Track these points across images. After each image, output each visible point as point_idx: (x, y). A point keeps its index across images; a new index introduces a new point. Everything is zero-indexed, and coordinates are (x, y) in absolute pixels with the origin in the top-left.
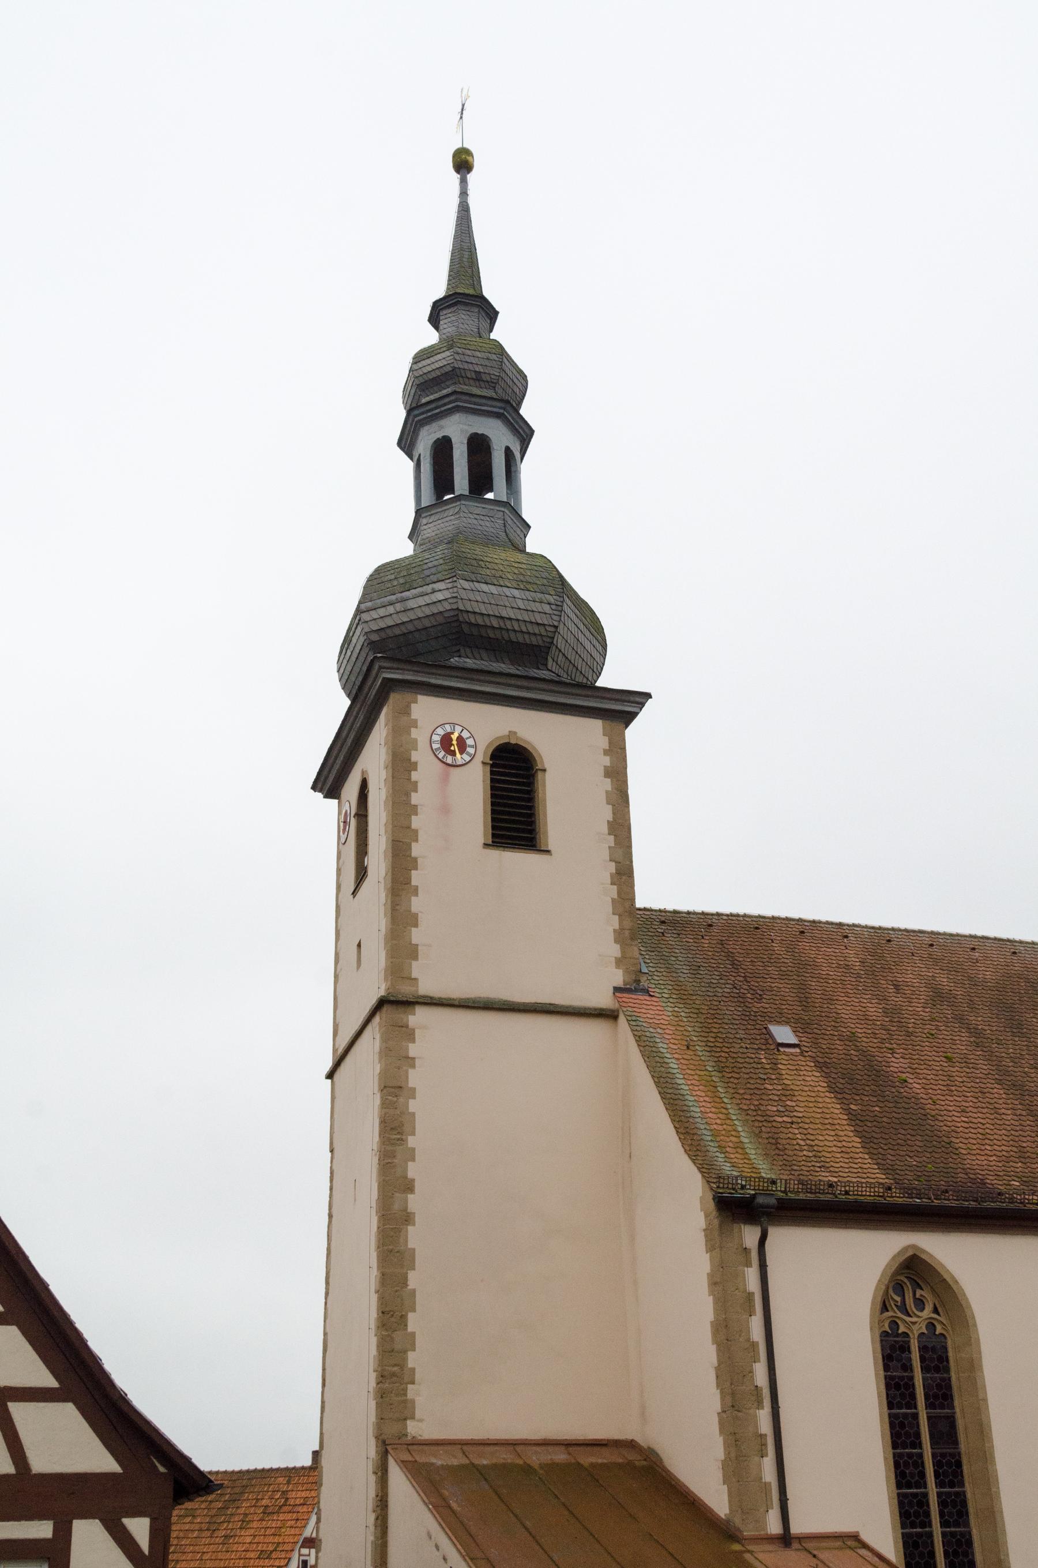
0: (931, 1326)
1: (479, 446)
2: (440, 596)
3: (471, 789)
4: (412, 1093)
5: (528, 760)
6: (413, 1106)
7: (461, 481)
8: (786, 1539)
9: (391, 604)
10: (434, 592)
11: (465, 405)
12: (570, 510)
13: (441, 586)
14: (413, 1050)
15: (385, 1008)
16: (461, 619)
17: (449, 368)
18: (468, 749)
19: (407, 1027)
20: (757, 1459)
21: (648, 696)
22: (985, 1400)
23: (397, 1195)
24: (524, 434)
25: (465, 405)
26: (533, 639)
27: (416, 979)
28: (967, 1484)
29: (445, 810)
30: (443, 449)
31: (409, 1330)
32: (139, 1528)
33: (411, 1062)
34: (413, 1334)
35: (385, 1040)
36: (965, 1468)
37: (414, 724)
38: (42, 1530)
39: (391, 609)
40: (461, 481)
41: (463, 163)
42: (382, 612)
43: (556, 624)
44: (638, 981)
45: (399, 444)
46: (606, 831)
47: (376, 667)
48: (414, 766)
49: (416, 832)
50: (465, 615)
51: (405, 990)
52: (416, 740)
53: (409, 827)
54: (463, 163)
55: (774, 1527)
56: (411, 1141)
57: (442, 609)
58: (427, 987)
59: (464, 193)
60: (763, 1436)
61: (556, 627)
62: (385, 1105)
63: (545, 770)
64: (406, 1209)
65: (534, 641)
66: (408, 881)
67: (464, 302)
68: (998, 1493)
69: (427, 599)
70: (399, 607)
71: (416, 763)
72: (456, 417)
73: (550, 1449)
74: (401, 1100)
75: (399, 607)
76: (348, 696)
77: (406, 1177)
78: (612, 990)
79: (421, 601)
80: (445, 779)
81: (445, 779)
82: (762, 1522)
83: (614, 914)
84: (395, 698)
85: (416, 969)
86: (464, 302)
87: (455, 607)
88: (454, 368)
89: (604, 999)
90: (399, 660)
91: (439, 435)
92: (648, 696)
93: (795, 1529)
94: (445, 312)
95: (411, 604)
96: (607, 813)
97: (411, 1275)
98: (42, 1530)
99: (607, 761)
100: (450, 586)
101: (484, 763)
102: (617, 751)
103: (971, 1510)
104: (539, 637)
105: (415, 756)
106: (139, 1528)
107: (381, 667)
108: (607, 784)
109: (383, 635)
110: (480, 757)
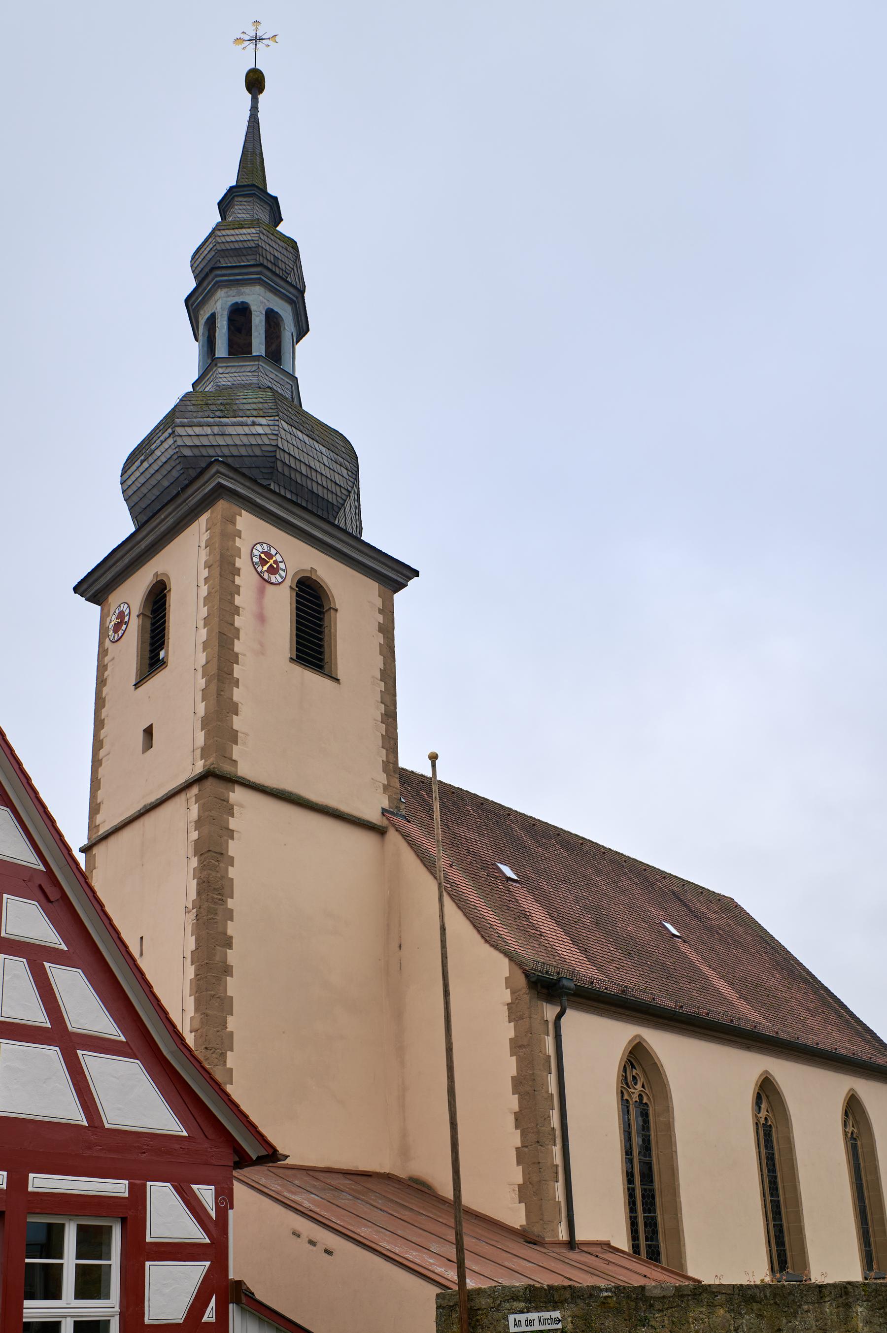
0: (640, 1096)
1: (272, 319)
2: (260, 430)
3: (281, 605)
4: (231, 861)
5: (318, 598)
6: (232, 872)
7: (258, 346)
8: (572, 1244)
9: (209, 425)
10: (254, 424)
11: (248, 281)
12: (327, 378)
13: (263, 421)
14: (233, 824)
15: (210, 783)
16: (278, 457)
17: (252, 244)
18: (281, 572)
19: (228, 802)
20: (552, 1183)
21: (416, 573)
22: (676, 1152)
23: (218, 948)
24: (295, 295)
25: (248, 281)
26: (330, 495)
27: (235, 761)
28: (658, 1212)
29: (261, 618)
30: (240, 315)
31: (228, 1066)
32: (206, 1194)
33: (231, 834)
34: (231, 1070)
35: (203, 808)
36: (657, 1199)
37: (239, 534)
38: (118, 1188)
39: (208, 430)
40: (258, 346)
41: (255, 82)
42: (198, 430)
43: (350, 489)
44: (398, 808)
45: (187, 301)
46: (379, 677)
47: (213, 470)
48: (237, 572)
49: (238, 630)
50: (282, 453)
51: (227, 768)
52: (239, 549)
53: (233, 625)
54: (255, 82)
55: (563, 1235)
56: (230, 903)
57: (260, 443)
58: (244, 770)
59: (254, 109)
60: (557, 1166)
61: (350, 492)
62: (203, 866)
63: (336, 610)
64: (225, 962)
65: (330, 497)
66: (231, 673)
67: (250, 192)
68: (681, 1217)
69: (247, 430)
70: (216, 430)
71: (239, 569)
72: (258, 289)
73: (334, 1175)
74: (222, 865)
75: (216, 430)
76: (135, 517)
77: (226, 934)
78: (380, 811)
79: (240, 430)
80: (261, 592)
81: (261, 592)
82: (555, 1232)
83: (383, 747)
84: (222, 505)
85: (237, 752)
86: (250, 192)
87: (274, 443)
88: (258, 246)
89: (373, 816)
90: (235, 470)
91: (239, 299)
92: (416, 573)
93: (580, 1236)
94: (240, 199)
95: (230, 430)
96: (379, 662)
97: (230, 1019)
98: (118, 1188)
99: (380, 618)
100: (271, 423)
101: (291, 588)
102: (388, 611)
103: (660, 1230)
104: (334, 496)
105: (239, 563)
106: (206, 1194)
107: (218, 472)
108: (380, 638)
109: (197, 452)
110: (288, 582)
